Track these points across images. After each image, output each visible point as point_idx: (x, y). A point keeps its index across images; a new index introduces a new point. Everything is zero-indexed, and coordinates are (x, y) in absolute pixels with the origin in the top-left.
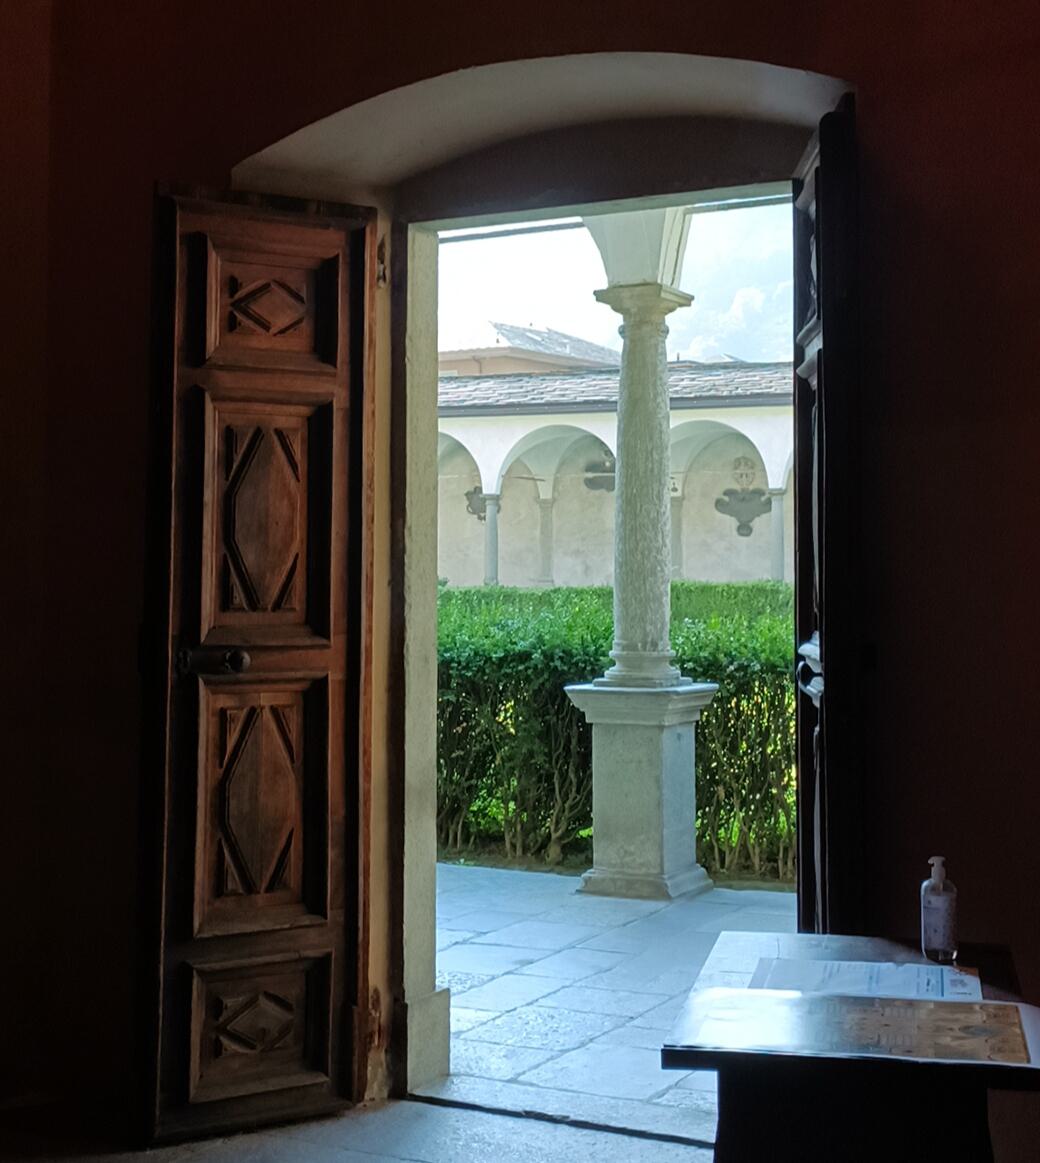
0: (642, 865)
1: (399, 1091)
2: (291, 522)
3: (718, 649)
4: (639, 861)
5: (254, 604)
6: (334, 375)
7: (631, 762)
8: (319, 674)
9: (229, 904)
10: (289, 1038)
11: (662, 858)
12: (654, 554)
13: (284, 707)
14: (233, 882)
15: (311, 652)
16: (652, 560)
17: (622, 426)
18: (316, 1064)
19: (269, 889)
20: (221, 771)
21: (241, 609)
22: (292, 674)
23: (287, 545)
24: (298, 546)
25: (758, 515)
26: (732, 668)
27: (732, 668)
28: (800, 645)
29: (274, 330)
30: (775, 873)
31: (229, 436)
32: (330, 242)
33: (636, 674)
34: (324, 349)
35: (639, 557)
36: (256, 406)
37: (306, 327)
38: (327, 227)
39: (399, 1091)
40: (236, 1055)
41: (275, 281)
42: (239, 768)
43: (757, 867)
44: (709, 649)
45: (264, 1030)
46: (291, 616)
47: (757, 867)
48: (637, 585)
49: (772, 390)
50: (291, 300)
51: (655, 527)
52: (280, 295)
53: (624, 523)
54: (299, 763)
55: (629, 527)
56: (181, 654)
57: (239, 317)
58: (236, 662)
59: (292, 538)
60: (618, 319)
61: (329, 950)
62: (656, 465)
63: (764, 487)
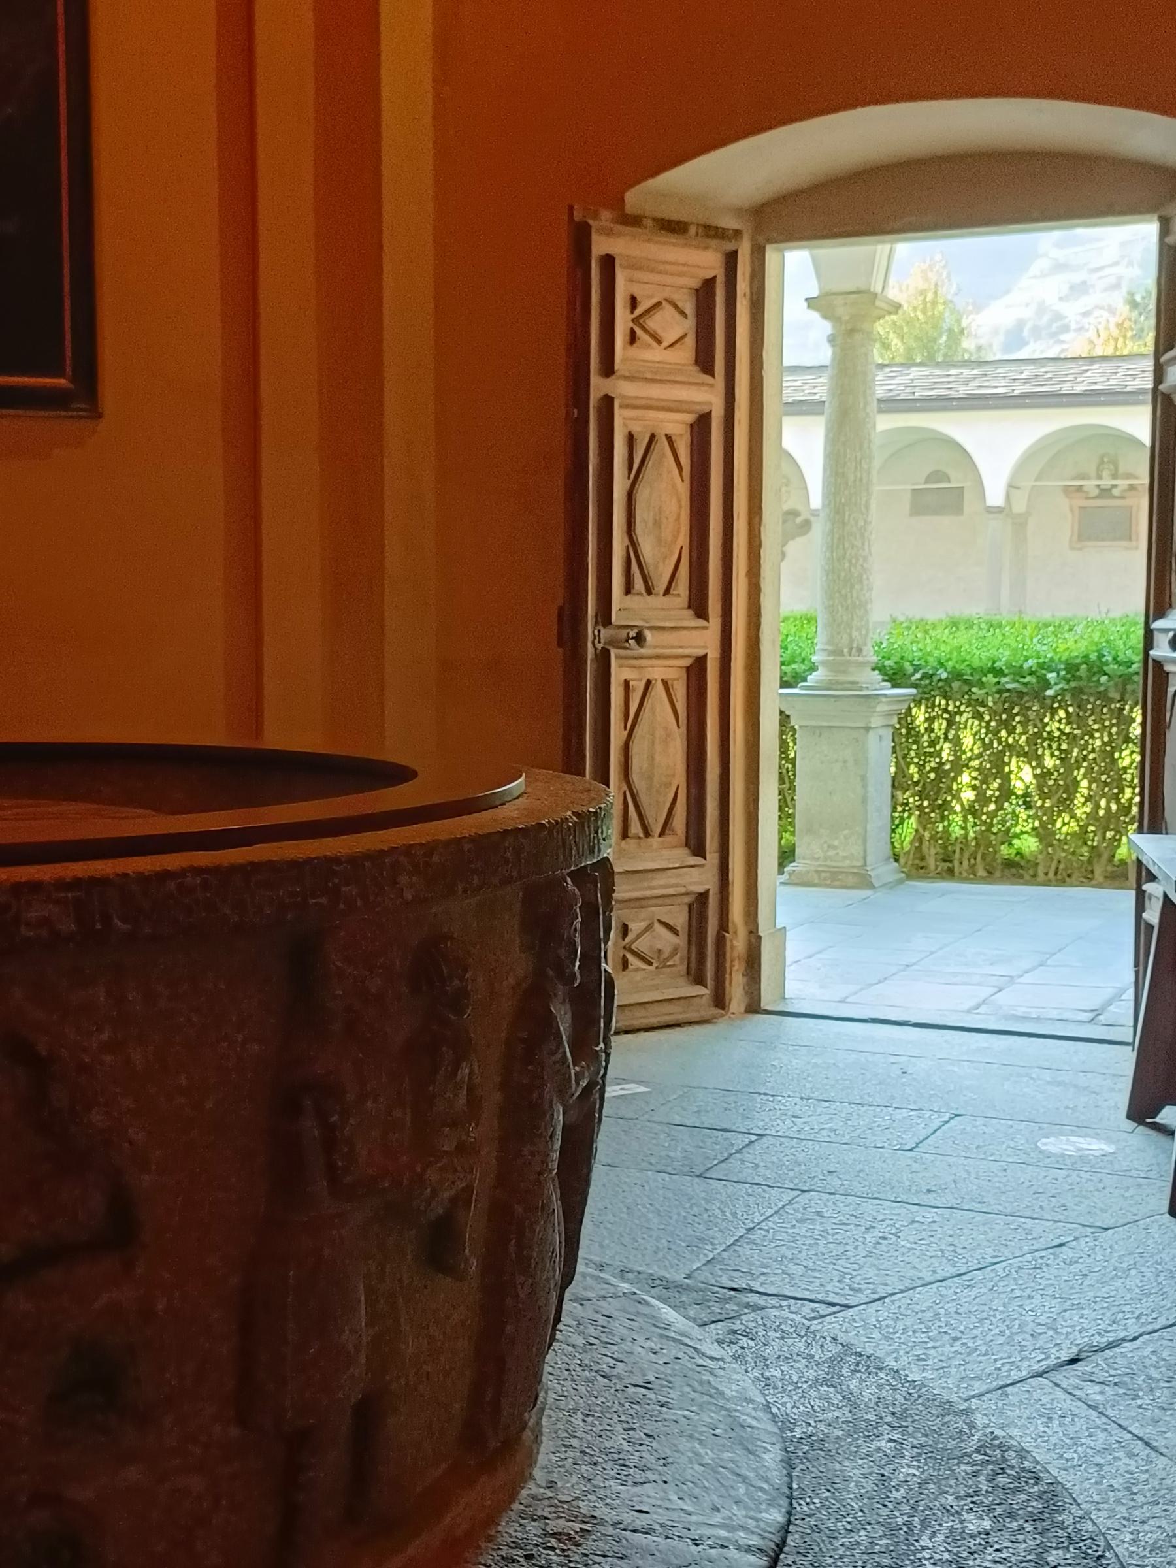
0: (845, 858)
1: (754, 1007)
2: (678, 518)
3: (902, 658)
4: (841, 854)
5: (649, 592)
6: (711, 386)
7: (837, 761)
8: (701, 652)
9: (630, 844)
10: (677, 958)
11: (865, 851)
12: (861, 562)
13: (674, 679)
14: (635, 828)
15: (695, 633)
16: (859, 567)
17: (831, 435)
18: (699, 980)
19: (661, 834)
20: (626, 733)
21: (640, 594)
22: (680, 651)
23: (675, 538)
24: (683, 539)
25: (793, 539)
26: (918, 676)
27: (918, 676)
28: (1154, 621)
29: (665, 344)
30: (951, 871)
31: (631, 438)
32: (709, 262)
33: (842, 678)
34: (704, 362)
35: (847, 565)
36: (652, 414)
37: (690, 341)
38: (706, 248)
39: (754, 1007)
40: (638, 969)
41: (666, 299)
42: (638, 731)
43: (932, 867)
44: (895, 658)
45: (659, 951)
46: (677, 600)
47: (932, 867)
48: (843, 592)
49: (817, 397)
50: (678, 316)
51: (862, 536)
52: (668, 310)
53: (832, 531)
54: (684, 729)
55: (837, 536)
56: (596, 632)
57: (639, 331)
58: (640, 639)
59: (678, 532)
60: (827, 327)
61: (707, 887)
62: (865, 475)
63: (800, 507)
